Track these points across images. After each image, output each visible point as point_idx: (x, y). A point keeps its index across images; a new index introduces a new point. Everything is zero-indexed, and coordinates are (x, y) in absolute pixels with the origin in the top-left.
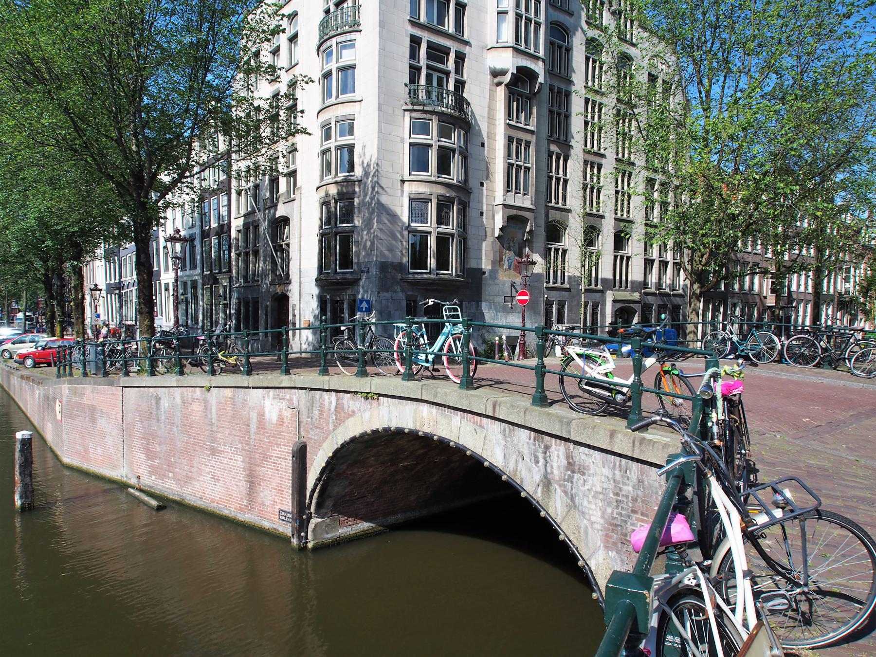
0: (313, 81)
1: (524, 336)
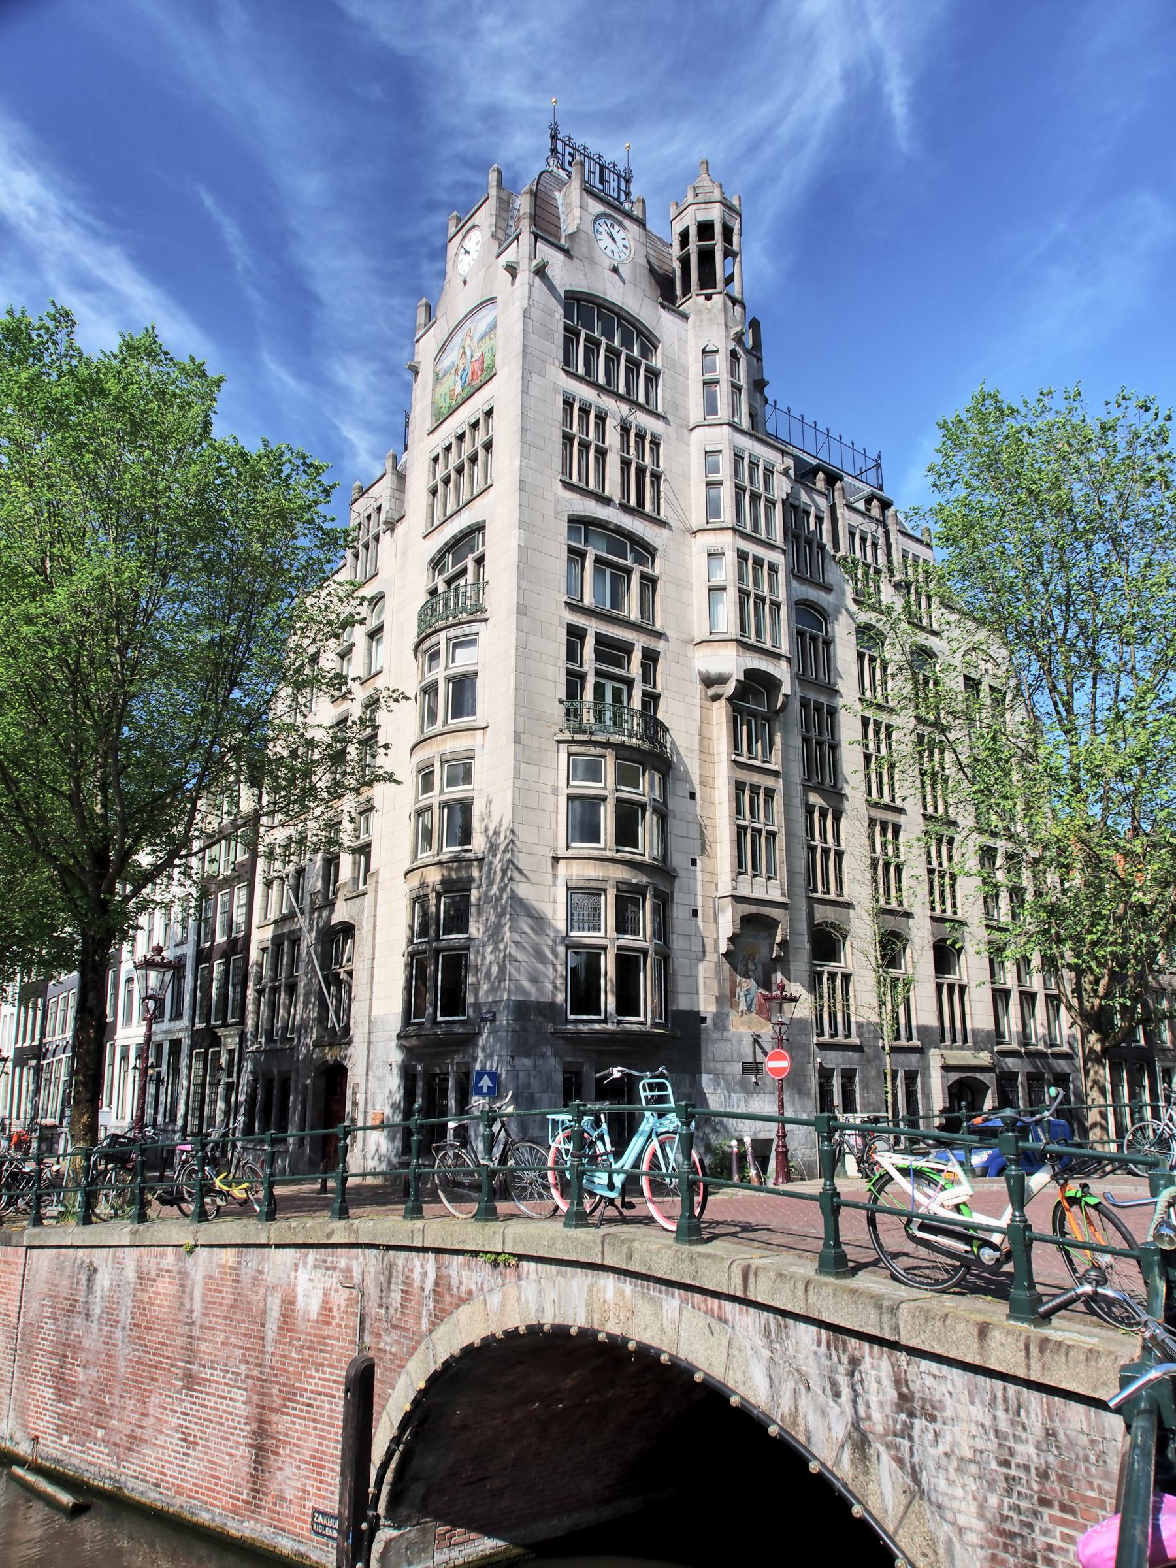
0: (406, 698)
1: (783, 1136)
